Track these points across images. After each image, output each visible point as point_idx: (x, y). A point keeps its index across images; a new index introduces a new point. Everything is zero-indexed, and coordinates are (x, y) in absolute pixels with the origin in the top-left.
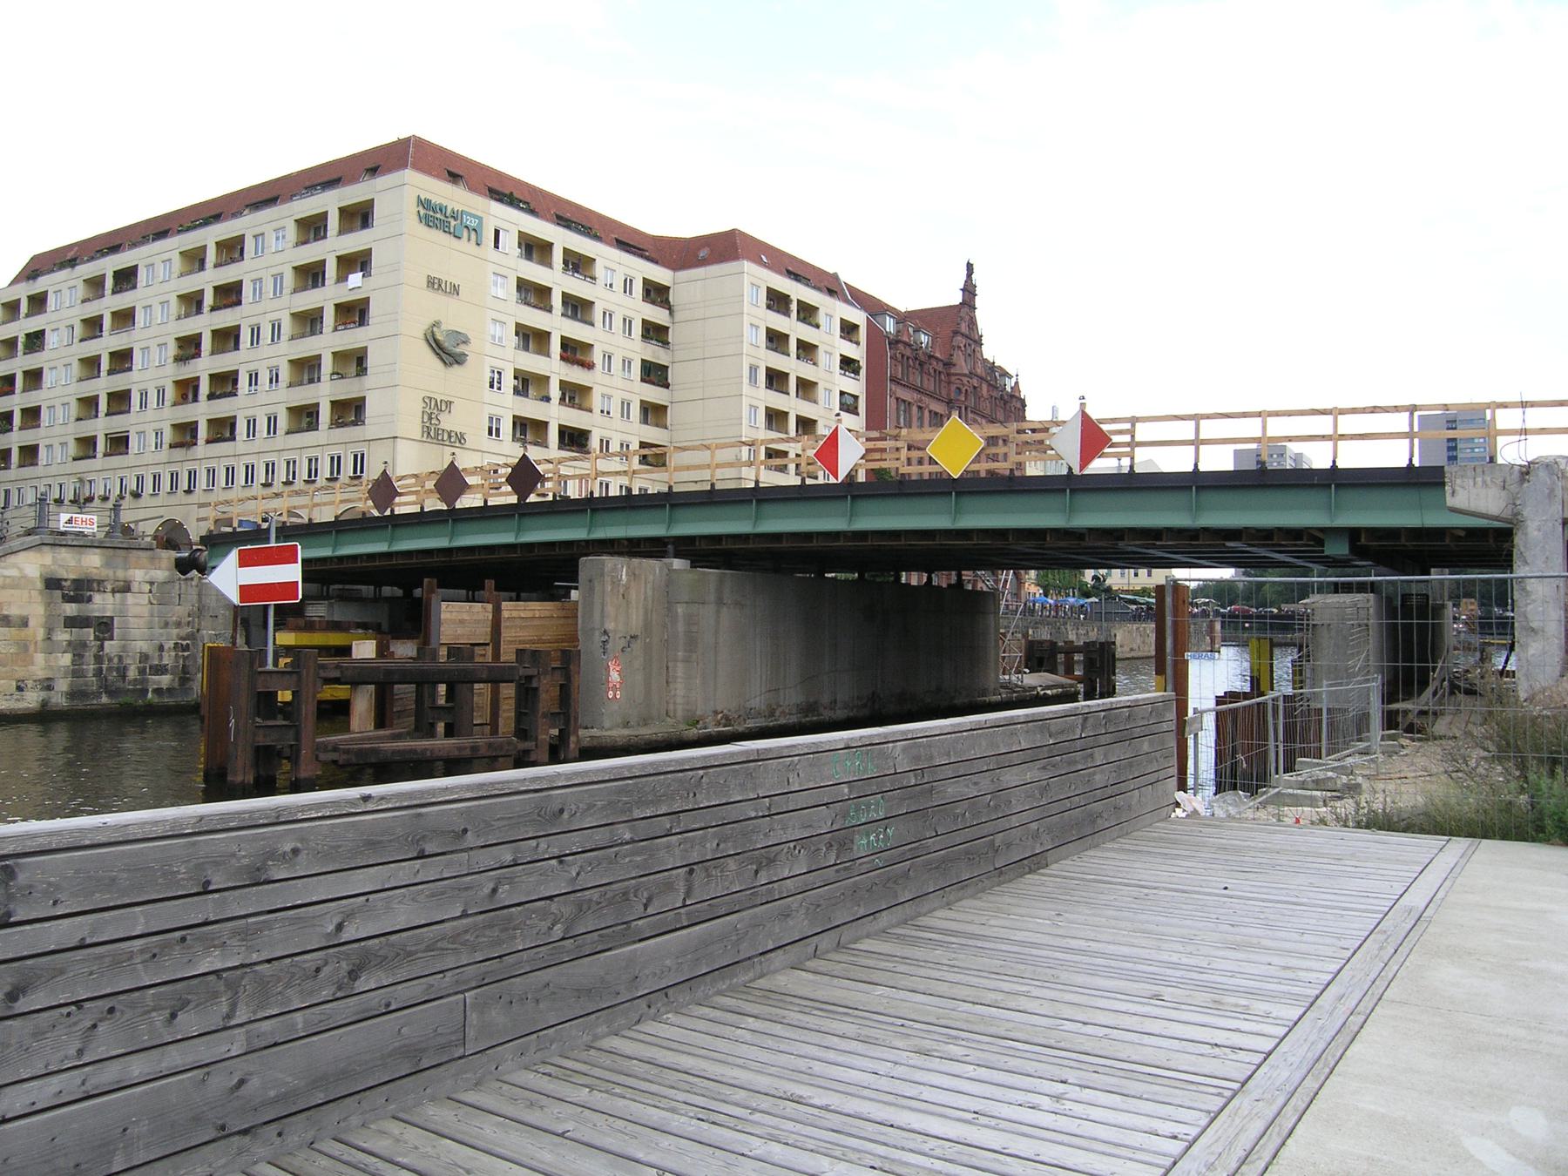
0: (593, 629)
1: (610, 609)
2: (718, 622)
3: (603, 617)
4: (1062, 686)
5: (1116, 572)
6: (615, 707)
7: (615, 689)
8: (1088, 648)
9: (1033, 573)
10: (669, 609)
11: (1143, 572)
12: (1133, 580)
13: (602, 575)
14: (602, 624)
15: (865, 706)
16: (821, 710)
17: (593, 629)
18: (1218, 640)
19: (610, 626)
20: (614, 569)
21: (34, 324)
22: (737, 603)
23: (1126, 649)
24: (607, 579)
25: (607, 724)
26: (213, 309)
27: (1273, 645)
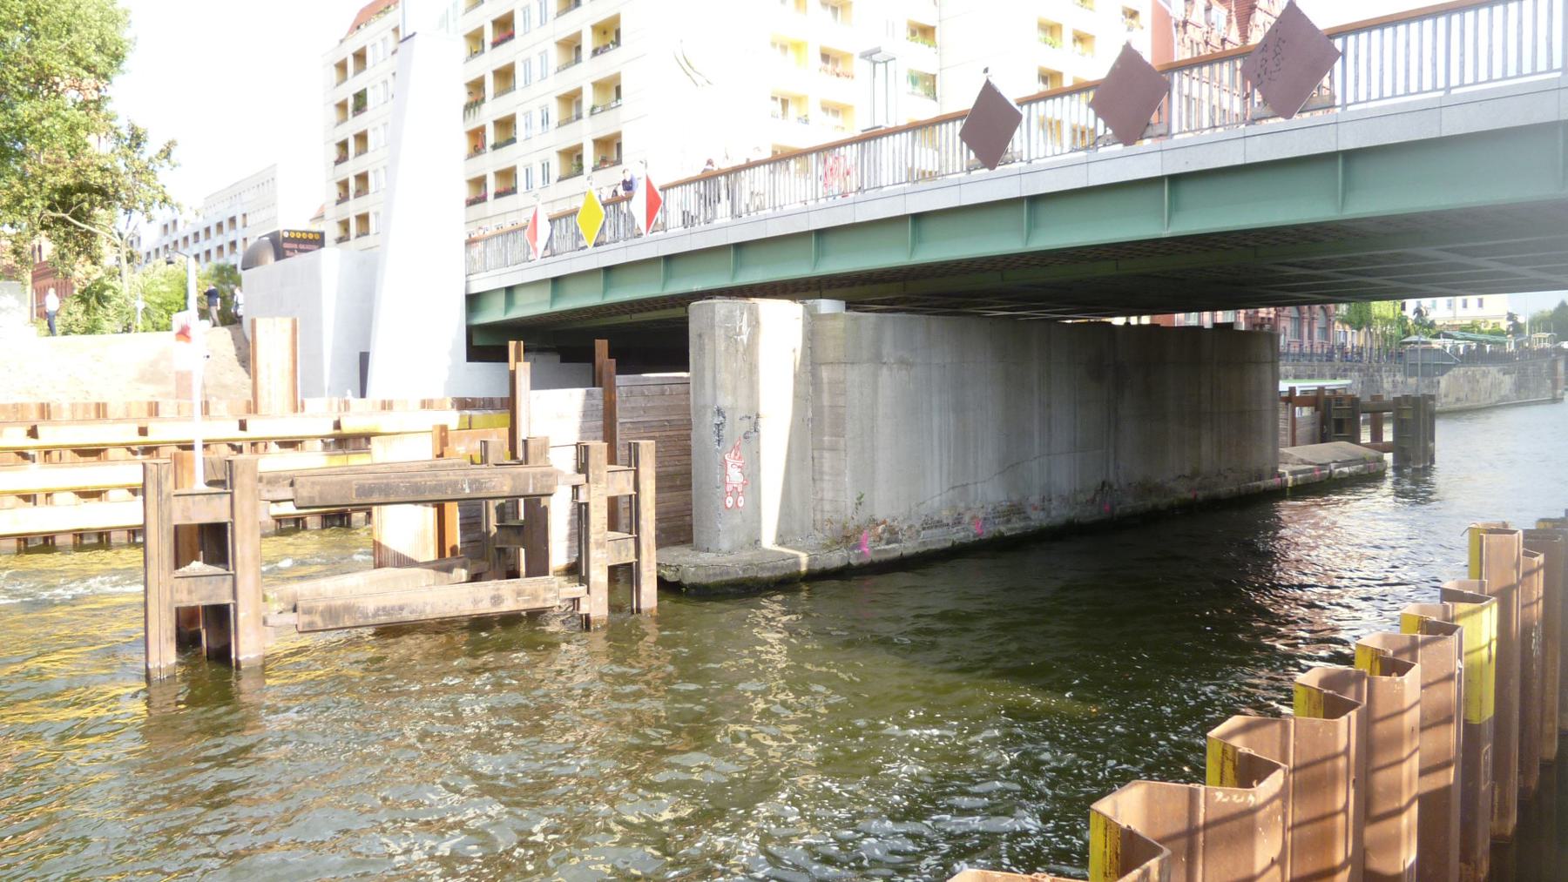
0: (705, 407)
1: (724, 377)
2: (875, 391)
3: (715, 387)
4: (1364, 460)
5: (1442, 302)
6: (737, 520)
7: (735, 493)
8: (1398, 405)
9: (1343, 308)
10: (813, 375)
11: (1473, 300)
12: (1460, 312)
13: (713, 327)
14: (715, 398)
15: (1093, 501)
16: (1030, 511)
17: (705, 407)
18: (1561, 384)
19: (725, 401)
20: (729, 317)
21: (601, 126)
22: (902, 362)
23: (1451, 399)
24: (720, 332)
25: (725, 544)
26: (495, 44)
27: (440, 506)
